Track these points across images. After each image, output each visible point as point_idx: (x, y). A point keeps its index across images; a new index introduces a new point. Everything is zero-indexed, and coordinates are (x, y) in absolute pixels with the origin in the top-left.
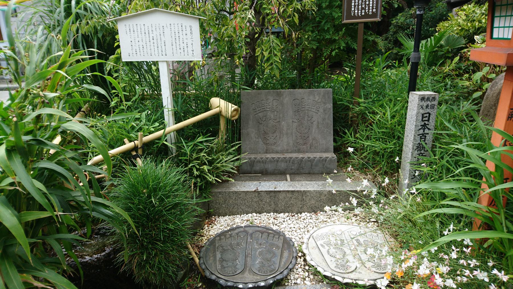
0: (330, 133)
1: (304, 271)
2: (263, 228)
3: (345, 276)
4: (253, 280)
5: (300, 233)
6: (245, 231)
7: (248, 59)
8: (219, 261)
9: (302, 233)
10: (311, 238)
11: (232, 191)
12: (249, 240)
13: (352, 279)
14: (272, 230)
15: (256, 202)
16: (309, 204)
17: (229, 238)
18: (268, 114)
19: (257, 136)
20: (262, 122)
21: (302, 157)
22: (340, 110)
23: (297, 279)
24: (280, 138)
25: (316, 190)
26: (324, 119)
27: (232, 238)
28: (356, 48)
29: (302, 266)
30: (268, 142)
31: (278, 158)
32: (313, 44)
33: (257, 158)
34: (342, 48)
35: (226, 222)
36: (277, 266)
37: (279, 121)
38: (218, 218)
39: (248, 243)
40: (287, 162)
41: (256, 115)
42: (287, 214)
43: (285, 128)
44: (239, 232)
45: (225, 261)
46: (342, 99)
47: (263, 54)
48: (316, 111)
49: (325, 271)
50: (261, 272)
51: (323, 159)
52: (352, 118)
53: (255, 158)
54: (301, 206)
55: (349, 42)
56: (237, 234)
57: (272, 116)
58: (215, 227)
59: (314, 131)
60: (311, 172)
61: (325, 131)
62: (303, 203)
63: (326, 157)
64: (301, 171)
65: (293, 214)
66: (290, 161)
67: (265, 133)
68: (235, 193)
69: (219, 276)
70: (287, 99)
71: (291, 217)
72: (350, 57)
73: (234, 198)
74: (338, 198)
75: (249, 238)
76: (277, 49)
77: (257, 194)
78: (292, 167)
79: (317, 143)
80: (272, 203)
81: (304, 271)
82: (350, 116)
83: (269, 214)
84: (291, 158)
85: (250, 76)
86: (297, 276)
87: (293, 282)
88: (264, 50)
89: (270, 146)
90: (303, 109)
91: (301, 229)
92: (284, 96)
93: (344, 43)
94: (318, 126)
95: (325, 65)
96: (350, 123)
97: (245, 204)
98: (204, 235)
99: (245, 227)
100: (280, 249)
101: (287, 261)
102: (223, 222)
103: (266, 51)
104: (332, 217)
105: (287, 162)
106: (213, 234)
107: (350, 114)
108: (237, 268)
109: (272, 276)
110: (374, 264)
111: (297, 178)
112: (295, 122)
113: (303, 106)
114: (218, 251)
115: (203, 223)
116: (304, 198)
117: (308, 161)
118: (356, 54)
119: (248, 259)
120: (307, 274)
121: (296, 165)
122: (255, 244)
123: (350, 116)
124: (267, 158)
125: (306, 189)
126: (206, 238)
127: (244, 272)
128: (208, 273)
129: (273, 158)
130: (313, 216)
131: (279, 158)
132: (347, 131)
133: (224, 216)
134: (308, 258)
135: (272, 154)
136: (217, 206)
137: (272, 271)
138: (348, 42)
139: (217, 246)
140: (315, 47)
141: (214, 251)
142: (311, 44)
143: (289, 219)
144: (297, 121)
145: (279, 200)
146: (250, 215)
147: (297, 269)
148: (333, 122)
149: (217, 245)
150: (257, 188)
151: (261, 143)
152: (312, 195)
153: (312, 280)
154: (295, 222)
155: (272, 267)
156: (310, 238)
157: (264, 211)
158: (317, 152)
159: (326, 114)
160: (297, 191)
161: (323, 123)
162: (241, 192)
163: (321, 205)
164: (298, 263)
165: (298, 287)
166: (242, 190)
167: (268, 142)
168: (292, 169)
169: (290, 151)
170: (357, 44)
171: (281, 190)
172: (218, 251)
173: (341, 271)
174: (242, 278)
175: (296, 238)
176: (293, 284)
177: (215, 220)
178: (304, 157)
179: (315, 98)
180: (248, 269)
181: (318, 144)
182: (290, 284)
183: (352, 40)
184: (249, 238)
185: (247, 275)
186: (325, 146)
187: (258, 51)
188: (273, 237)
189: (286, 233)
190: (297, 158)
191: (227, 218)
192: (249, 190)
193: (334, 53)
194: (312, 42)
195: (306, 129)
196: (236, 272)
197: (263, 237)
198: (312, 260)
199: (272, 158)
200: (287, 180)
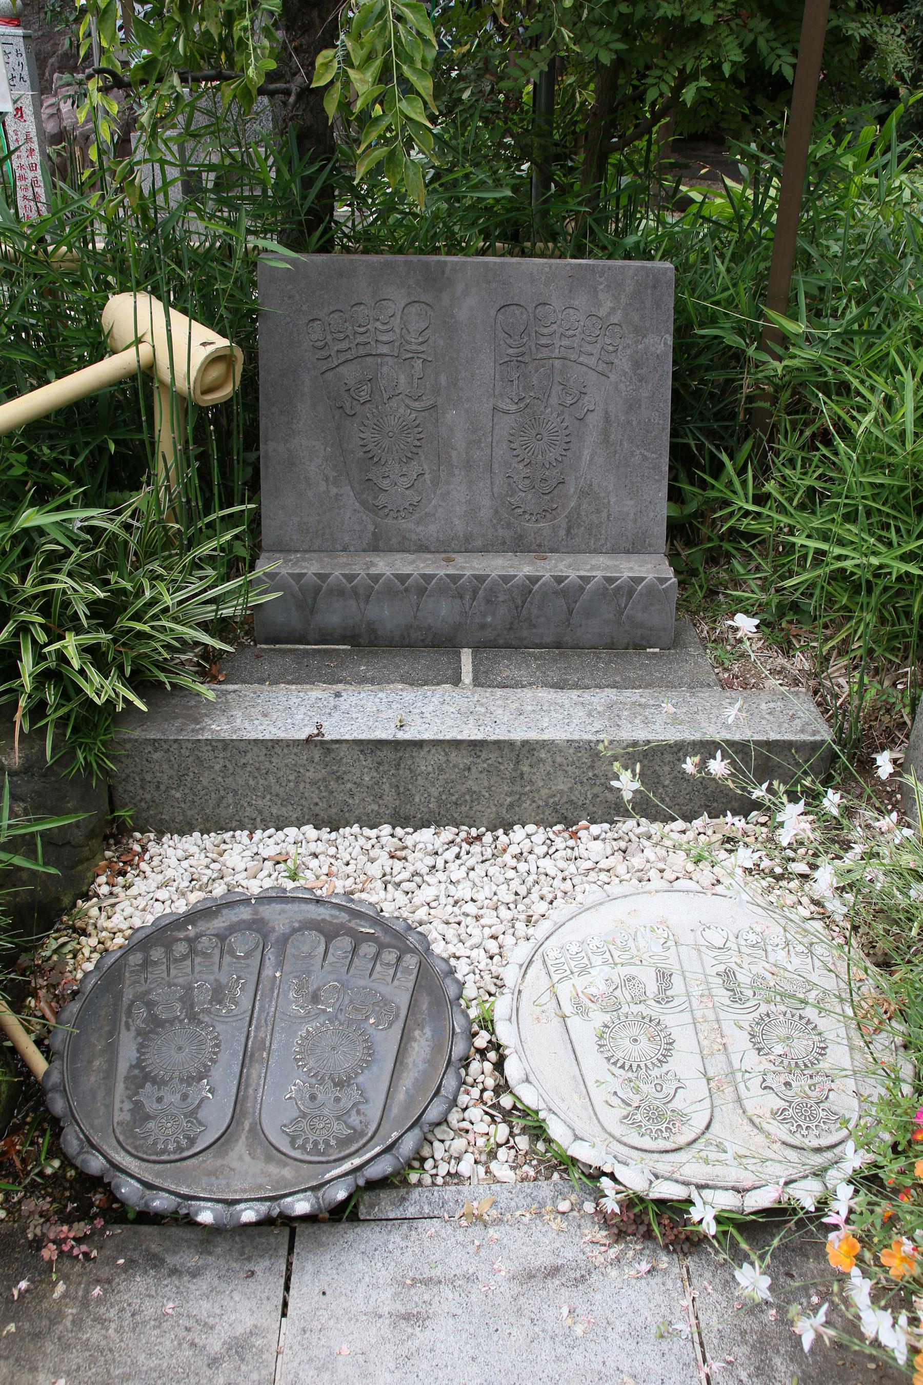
0: (656, 468)
1: (492, 1116)
2: (337, 906)
3: (664, 1165)
4: (261, 1187)
5: (493, 931)
6: (258, 926)
7: (292, 99)
8: (127, 1078)
9: (502, 928)
10: (537, 964)
11: (207, 736)
12: (268, 972)
13: (686, 1184)
14: (377, 920)
15: (313, 783)
16: (545, 792)
17: (184, 957)
18: (385, 369)
19: (332, 474)
20: (358, 408)
21: (528, 578)
22: (704, 360)
23: (459, 1159)
24: (436, 482)
25: (576, 737)
26: (632, 405)
27: (198, 960)
28: (788, 72)
29: (488, 1095)
30: (382, 499)
31: (423, 576)
32: (597, 43)
33: (327, 576)
34: (727, 69)
35: (185, 864)
36: (374, 1112)
37: (434, 407)
38: (158, 841)
39: (265, 984)
40: (461, 597)
41: (330, 375)
42: (448, 833)
43: (459, 441)
44: (233, 928)
45: (154, 1081)
46: (714, 312)
47: (347, 83)
48: (601, 367)
49: (577, 1138)
50: (303, 1147)
51: (619, 588)
52: (750, 399)
53: (323, 577)
54: (509, 800)
55: (761, 43)
56: (222, 937)
57: (402, 379)
58: (140, 886)
59: (586, 453)
60: (567, 638)
61: (637, 459)
62: (517, 788)
63: (632, 578)
64: (525, 633)
65: (474, 832)
66: (475, 592)
67: (370, 459)
68: (220, 746)
69: (122, 1159)
70: (471, 301)
71: (465, 846)
72: (760, 113)
73: (217, 767)
74: (667, 769)
75: (271, 958)
76: (418, 58)
77: (317, 754)
78: (484, 616)
79: (598, 511)
80: (386, 787)
81: (492, 1116)
82: (746, 391)
83: (373, 833)
84: (481, 579)
85: (307, 183)
86: (459, 1144)
87: (443, 1169)
88: (356, 63)
89: (389, 521)
90: (545, 353)
91: (502, 909)
92: (460, 287)
93: (741, 45)
94: (606, 433)
95: (649, 142)
96: (741, 417)
97: (268, 789)
98: (90, 929)
99: (264, 899)
100: (398, 1026)
101: (420, 1085)
102: (173, 862)
103: (362, 68)
104: (634, 845)
105: (461, 597)
106: (124, 926)
107: (745, 383)
108: (200, 1123)
109: (347, 1166)
110: (784, 1104)
111: (507, 669)
112: (506, 413)
113: (543, 341)
114: (128, 1028)
115: (88, 869)
116: (526, 769)
117: (556, 593)
118: (788, 103)
119: (254, 1074)
120: (502, 1131)
121: (502, 610)
122: (292, 994)
123: (746, 391)
124: (376, 578)
125: (533, 735)
126: (93, 941)
127: (227, 1140)
128: (75, 1143)
129: (403, 578)
130: (559, 843)
131: (428, 578)
132: (724, 458)
133: (182, 833)
134: (512, 1069)
135: (399, 556)
136: (148, 797)
137: (349, 1140)
138: (754, 43)
139: (126, 1000)
140: (606, 58)
141: (113, 1032)
142: (589, 40)
143: (458, 857)
144: (513, 408)
145: (414, 778)
146: (292, 831)
147: (464, 1110)
148: (673, 413)
149: (128, 994)
150: (319, 727)
151: (350, 500)
152: (559, 759)
153: (521, 1159)
154: (480, 870)
155: (354, 1120)
156: (531, 962)
157: (352, 819)
158: (596, 551)
159: (641, 379)
160: (497, 743)
161: (629, 422)
162: (249, 741)
163: (596, 796)
164: (470, 1080)
165: (459, 1192)
166: (252, 736)
167: (382, 499)
168: (483, 626)
169: (479, 543)
170: (795, 53)
171: (426, 736)
172: (128, 1028)
173: (647, 1143)
174: (214, 1173)
175: (474, 954)
176: (440, 1181)
177: (145, 850)
178: (538, 578)
179: (599, 305)
180: (247, 1125)
181: (604, 514)
182: (427, 1180)
183: (772, 35)
184: (271, 958)
185: (241, 1159)
186: (630, 525)
187: (327, 65)
188: (377, 955)
189: (433, 932)
190: (506, 579)
191: (191, 842)
192: (282, 735)
193: (689, 95)
194: (593, 31)
195: (552, 444)
196: (192, 1141)
197: (330, 958)
198: (527, 1080)
199: (397, 576)
200: (456, 681)
